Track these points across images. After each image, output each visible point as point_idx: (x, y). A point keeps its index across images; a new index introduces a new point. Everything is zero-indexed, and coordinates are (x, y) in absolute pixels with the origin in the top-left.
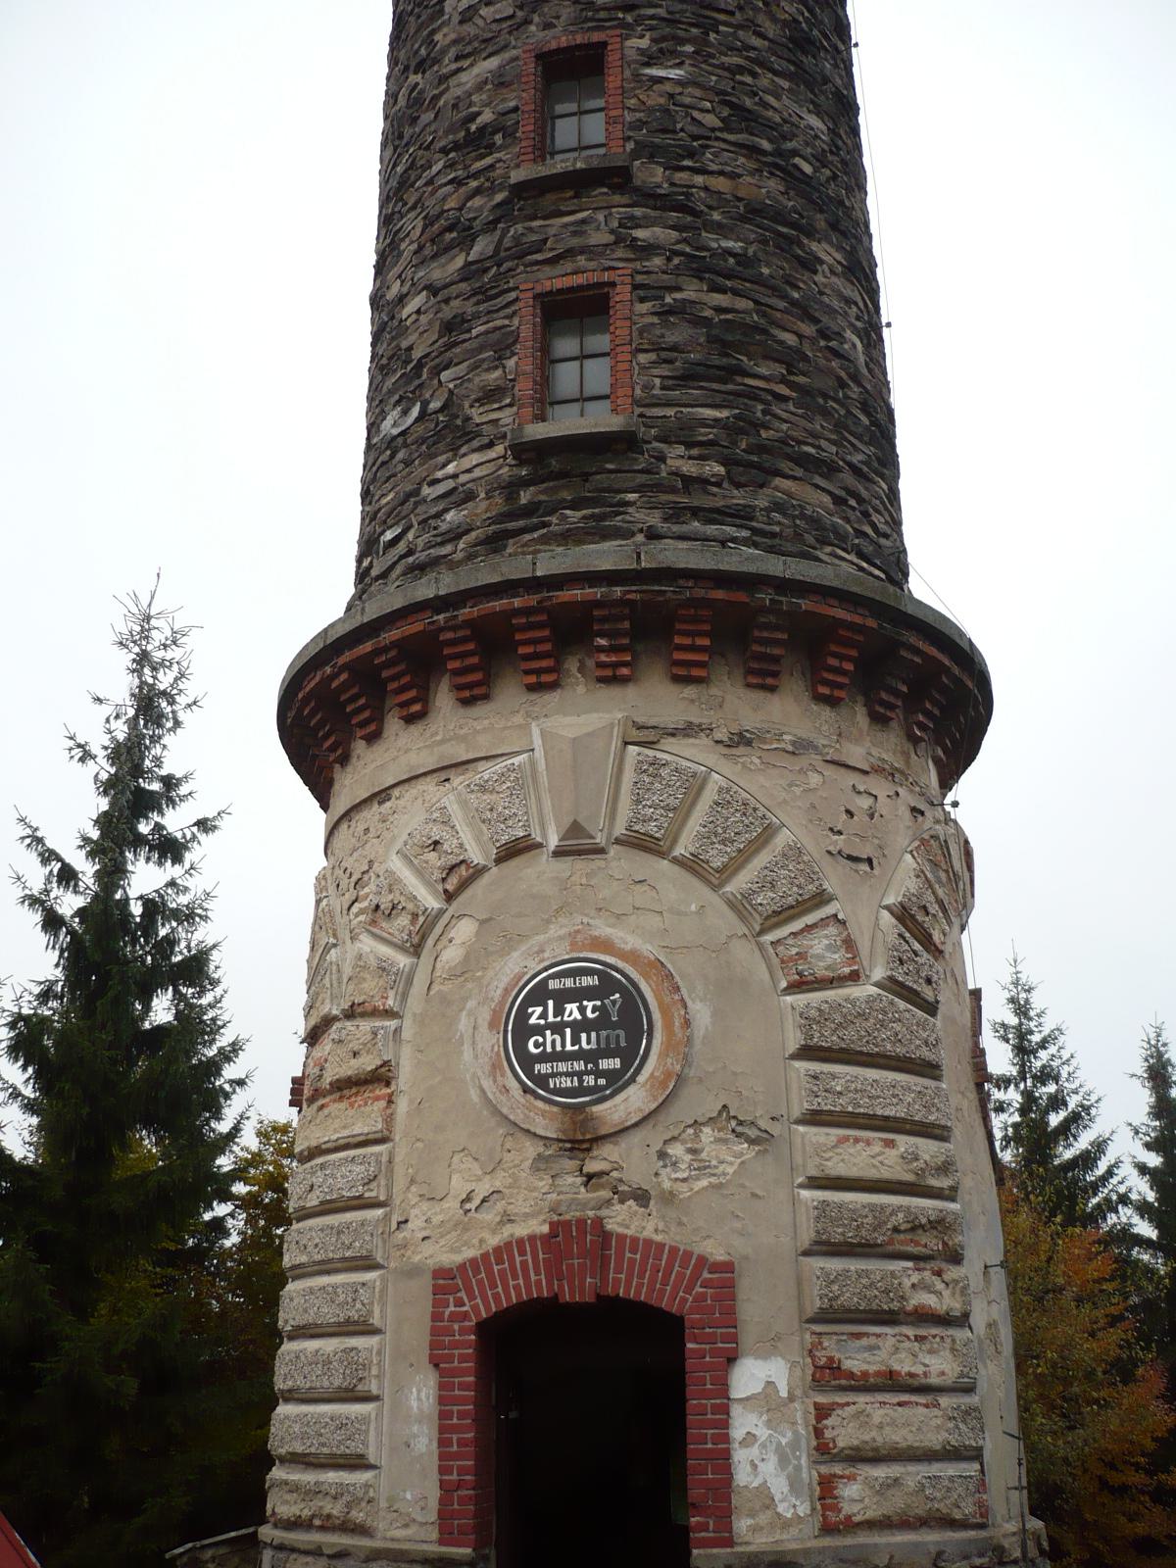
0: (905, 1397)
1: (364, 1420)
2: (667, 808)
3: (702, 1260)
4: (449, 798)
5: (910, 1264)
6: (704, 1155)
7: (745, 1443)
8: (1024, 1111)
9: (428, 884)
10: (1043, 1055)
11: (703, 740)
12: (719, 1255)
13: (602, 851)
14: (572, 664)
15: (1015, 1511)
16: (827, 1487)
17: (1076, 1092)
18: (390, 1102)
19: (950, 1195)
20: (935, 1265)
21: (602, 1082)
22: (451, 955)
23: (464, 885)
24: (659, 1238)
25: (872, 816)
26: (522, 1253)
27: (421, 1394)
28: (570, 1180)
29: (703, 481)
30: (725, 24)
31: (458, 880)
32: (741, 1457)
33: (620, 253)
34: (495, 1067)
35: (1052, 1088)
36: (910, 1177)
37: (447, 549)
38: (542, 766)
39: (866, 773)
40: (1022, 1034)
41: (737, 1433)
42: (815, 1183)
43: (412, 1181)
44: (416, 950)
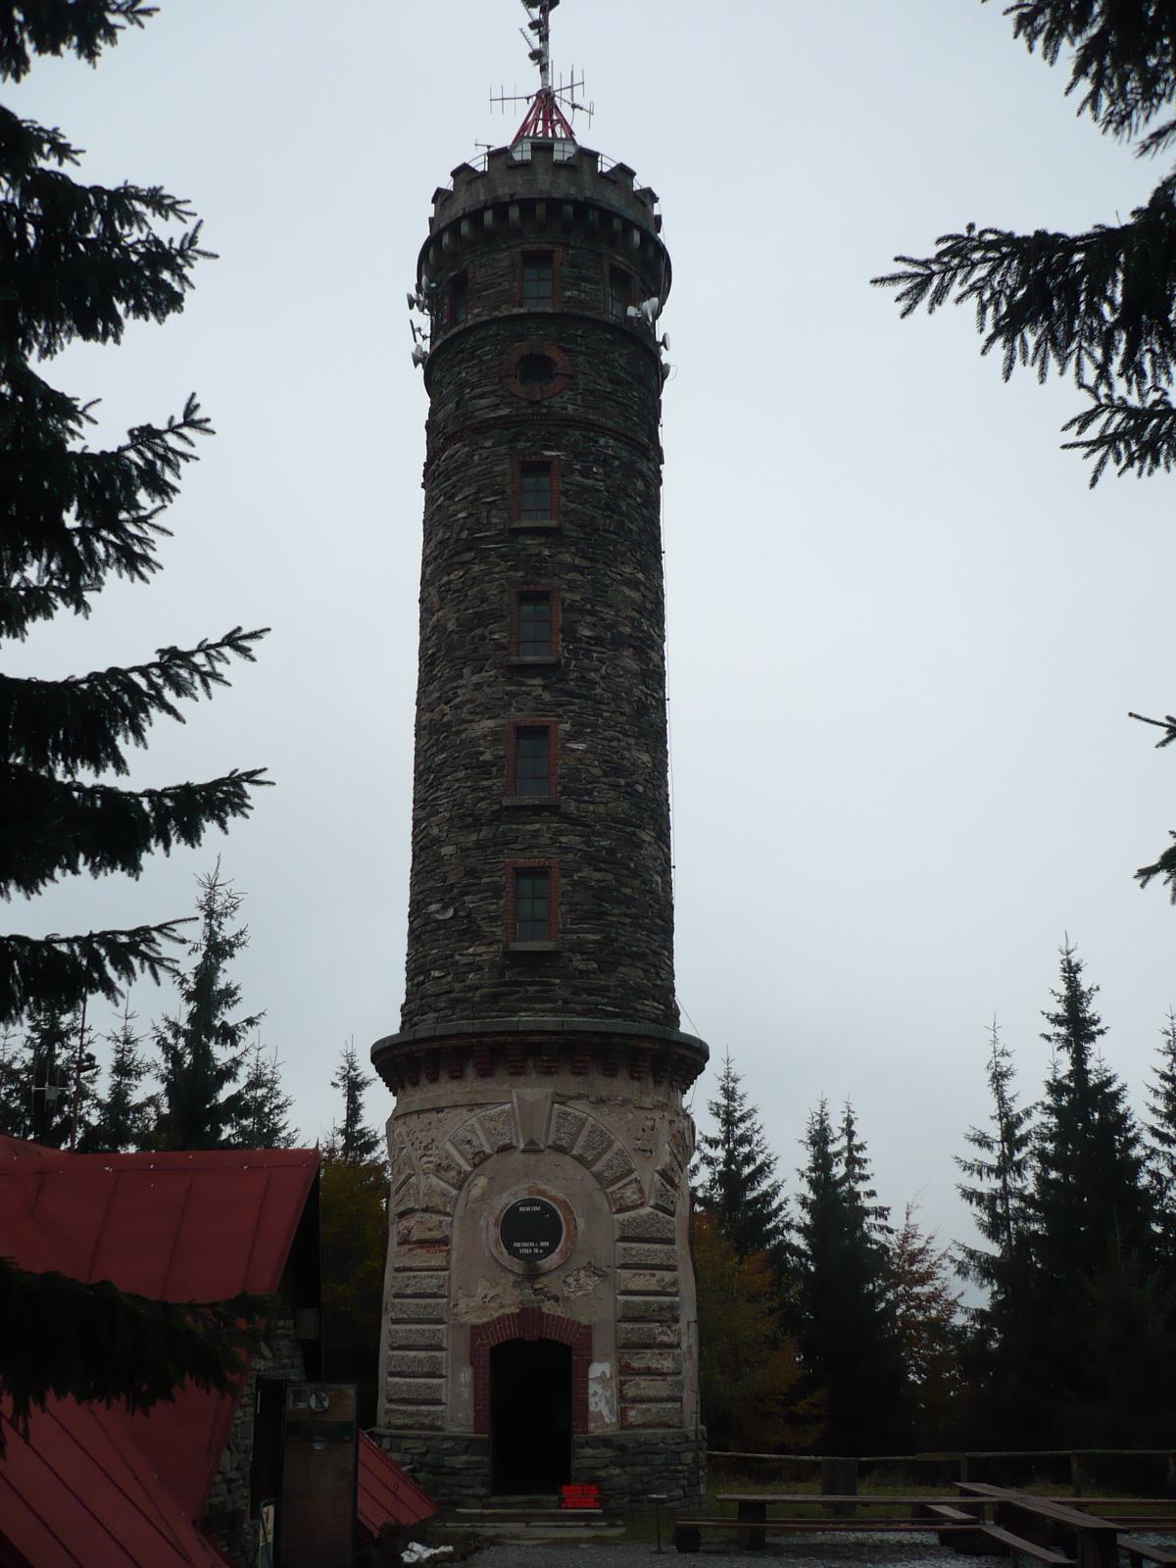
0: (654, 1377)
1: (440, 1385)
2: (570, 1134)
3: (579, 1324)
4: (473, 1119)
5: (658, 1324)
6: (581, 1282)
7: (595, 1394)
8: (727, 1163)
9: (467, 1160)
10: (742, 1125)
11: (585, 1101)
12: (584, 1321)
13: (542, 1151)
14: (530, 1063)
15: (694, 1422)
16: (622, 1414)
17: (762, 1152)
18: (448, 1253)
19: (676, 1294)
20: (668, 1324)
21: (541, 1251)
22: (476, 1192)
23: (482, 1161)
24: (563, 1315)
25: (652, 1130)
26: (509, 1320)
27: (466, 1375)
28: (527, 1291)
29: (587, 972)
30: (607, 711)
31: (479, 1159)
32: (592, 1400)
33: (554, 850)
34: (497, 1243)
35: (746, 1149)
36: (660, 1289)
37: (471, 995)
38: (517, 1112)
39: (651, 1109)
40: (729, 1113)
41: (591, 1391)
42: (623, 1293)
43: (460, 1288)
44: (460, 1188)
